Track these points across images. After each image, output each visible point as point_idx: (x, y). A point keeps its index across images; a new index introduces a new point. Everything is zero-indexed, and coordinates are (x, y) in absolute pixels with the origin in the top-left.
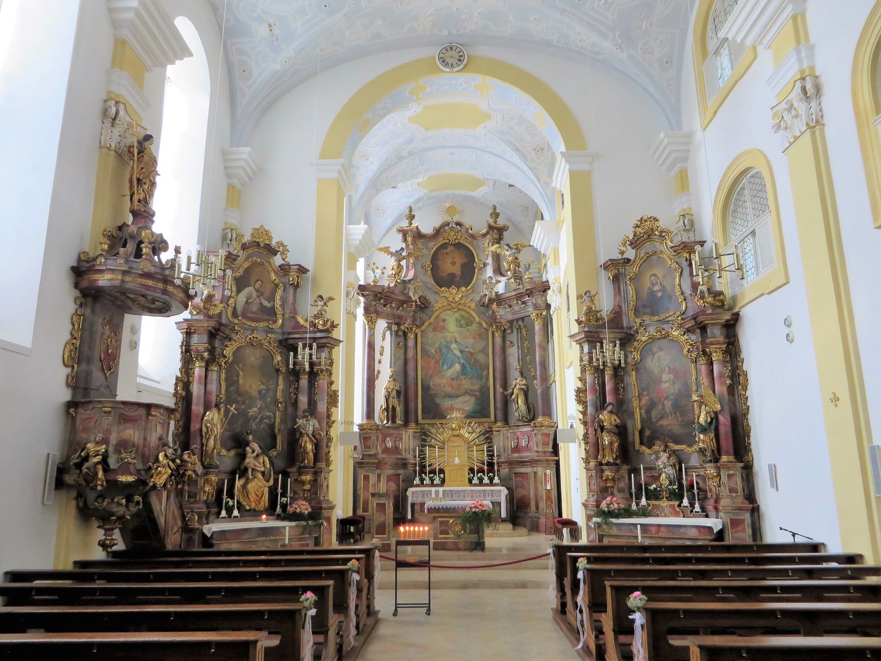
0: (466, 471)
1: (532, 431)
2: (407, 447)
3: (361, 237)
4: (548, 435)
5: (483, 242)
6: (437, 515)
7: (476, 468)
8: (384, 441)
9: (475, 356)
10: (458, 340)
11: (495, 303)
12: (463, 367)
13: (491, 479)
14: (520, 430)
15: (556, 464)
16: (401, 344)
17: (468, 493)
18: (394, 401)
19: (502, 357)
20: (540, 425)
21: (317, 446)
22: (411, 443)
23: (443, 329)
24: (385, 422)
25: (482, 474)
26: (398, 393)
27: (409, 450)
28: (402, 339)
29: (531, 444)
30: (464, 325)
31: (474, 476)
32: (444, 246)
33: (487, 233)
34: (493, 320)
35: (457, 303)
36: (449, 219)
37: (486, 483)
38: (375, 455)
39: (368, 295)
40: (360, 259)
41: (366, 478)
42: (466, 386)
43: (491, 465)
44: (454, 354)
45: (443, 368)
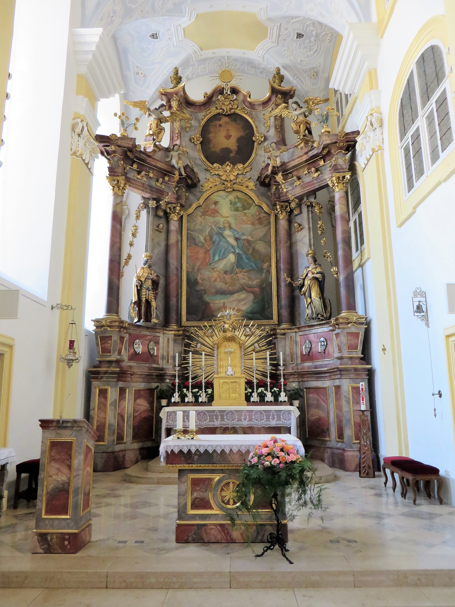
0: (243, 385)
2: (165, 354)
3: (94, 48)
4: (356, 335)
5: (263, 112)
6: (186, 467)
7: (255, 381)
8: (132, 343)
10: (233, 226)
11: (280, 174)
12: (239, 257)
13: (276, 396)
14: (314, 331)
16: (161, 225)
17: (245, 415)
18: (147, 294)
19: (288, 244)
20: (345, 321)
21: (318, 439)
23: (215, 212)
24: (136, 320)
25: (263, 389)
26: (155, 284)
27: (168, 356)
28: (163, 221)
29: (329, 348)
30: (240, 209)
31: (253, 392)
32: (216, 117)
33: (269, 99)
34: (277, 198)
36: (224, 85)
37: (269, 401)
38: (118, 362)
39: (114, 152)
40: (100, 99)
41: (103, 393)
42: (242, 281)
43: (275, 377)
44: (227, 242)
45: (213, 259)
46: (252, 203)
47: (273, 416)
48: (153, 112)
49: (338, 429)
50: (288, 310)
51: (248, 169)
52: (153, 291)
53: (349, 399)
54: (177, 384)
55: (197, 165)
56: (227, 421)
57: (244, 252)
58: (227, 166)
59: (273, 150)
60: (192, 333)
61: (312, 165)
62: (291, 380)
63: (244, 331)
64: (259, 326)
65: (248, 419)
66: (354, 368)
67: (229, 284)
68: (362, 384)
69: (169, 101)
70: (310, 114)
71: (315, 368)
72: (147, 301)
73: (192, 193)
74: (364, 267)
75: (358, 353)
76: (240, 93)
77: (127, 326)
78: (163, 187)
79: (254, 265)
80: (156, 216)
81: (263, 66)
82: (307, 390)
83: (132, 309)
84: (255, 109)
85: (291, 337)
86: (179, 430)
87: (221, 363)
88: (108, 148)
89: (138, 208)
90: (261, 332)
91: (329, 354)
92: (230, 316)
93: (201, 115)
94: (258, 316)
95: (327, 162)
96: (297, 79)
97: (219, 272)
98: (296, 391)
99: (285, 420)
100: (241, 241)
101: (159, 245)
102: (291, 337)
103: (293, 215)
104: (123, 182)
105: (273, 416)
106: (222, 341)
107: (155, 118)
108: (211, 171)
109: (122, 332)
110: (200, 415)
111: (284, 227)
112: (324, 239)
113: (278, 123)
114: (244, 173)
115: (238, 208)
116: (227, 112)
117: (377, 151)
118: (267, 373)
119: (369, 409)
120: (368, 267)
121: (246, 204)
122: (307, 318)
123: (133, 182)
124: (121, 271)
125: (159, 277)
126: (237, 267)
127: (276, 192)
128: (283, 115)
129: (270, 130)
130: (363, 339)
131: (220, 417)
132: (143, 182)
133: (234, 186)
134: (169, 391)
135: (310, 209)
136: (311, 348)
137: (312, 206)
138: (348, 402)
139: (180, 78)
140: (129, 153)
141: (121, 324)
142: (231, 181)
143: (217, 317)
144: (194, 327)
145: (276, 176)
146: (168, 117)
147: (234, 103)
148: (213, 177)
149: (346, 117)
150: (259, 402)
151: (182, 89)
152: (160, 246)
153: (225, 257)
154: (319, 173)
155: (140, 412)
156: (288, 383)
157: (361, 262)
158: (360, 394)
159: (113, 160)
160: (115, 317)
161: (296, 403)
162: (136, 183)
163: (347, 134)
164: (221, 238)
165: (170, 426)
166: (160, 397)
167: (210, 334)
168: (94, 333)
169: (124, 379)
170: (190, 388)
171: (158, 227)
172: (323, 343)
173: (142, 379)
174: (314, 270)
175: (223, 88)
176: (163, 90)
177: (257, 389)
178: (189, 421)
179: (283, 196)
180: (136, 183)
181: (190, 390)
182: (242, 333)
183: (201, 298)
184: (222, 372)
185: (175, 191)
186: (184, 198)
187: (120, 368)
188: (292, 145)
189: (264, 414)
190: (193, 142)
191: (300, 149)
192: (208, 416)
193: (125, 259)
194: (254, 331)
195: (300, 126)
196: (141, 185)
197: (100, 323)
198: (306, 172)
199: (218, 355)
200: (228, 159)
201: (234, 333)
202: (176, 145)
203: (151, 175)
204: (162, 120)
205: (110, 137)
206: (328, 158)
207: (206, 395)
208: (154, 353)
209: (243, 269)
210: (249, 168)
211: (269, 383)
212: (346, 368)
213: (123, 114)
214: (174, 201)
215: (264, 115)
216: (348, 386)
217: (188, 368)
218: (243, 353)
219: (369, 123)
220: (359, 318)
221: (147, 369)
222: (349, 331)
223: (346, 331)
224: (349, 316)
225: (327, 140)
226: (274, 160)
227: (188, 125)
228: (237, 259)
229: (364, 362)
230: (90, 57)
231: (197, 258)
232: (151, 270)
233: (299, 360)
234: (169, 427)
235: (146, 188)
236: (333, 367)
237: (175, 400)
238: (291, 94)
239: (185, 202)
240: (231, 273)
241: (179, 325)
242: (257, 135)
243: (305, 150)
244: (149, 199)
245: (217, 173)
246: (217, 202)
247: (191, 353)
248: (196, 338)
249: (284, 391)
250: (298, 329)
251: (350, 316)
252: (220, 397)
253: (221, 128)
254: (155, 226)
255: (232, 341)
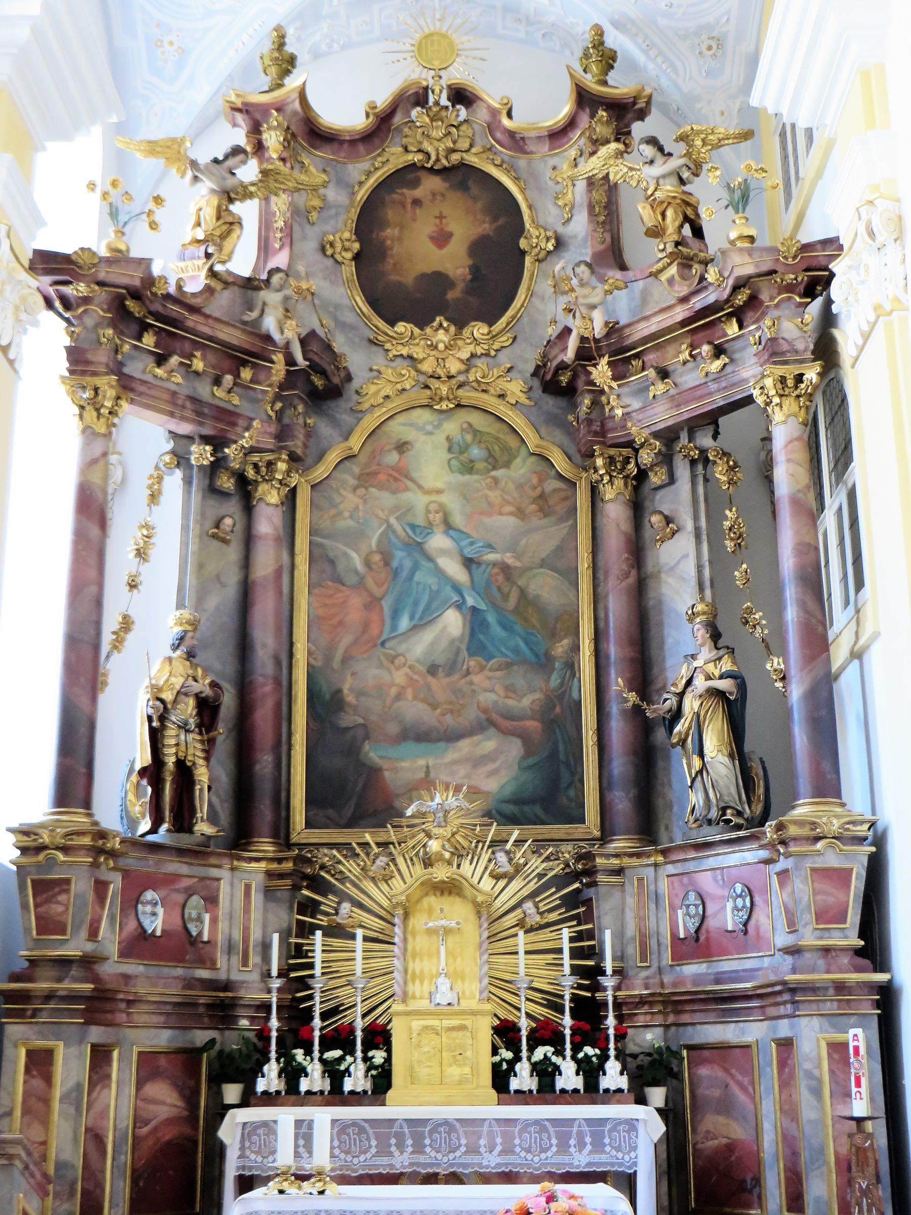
0: (486, 1037)
1: (767, 862)
4: (842, 877)
5: (552, 162)
7: (525, 1025)
8: (131, 901)
9: (521, 582)
10: (458, 520)
11: (604, 361)
14: (711, 862)
15: (878, 1004)
16: (228, 521)
17: (491, 1136)
19: (632, 580)
20: (805, 831)
22: (256, 915)
24: (145, 825)
25: (549, 1050)
28: (233, 507)
29: (761, 918)
30: (481, 466)
33: (571, 124)
34: (596, 434)
35: (454, 381)
36: (426, 78)
37: (569, 1087)
38: (88, 962)
39: (86, 300)
40: (48, 144)
42: (487, 698)
44: (440, 573)
45: (394, 627)
46: (519, 447)
47: (580, 1136)
48: (207, 171)
49: (787, 1179)
50: (633, 792)
51: (504, 338)
52: (201, 733)
53: (820, 1080)
54: (274, 1034)
55: (342, 326)
56: (433, 1154)
57: (494, 605)
58: (437, 330)
59: (582, 284)
60: (323, 867)
61: (701, 335)
62: (641, 1020)
63: (490, 860)
64: (540, 844)
65: (499, 1148)
66: (834, 982)
67: (445, 706)
68: (855, 1035)
69: (255, 130)
70: (697, 175)
71: (718, 981)
72: (180, 764)
73: (326, 415)
74: (866, 658)
75: (848, 933)
76: (479, 103)
77: (117, 846)
78: (236, 401)
79: (522, 645)
80: (213, 490)
81: (552, 19)
82: (693, 1053)
83: (132, 789)
84: (525, 152)
85: (640, 880)
86: (284, 1169)
87: (415, 966)
88: (68, 290)
89: (157, 468)
90: (545, 865)
91: (758, 936)
92: (446, 812)
93: (356, 170)
94: (538, 810)
95: (748, 326)
96: (659, 60)
97: (410, 667)
98: (656, 1056)
99: (618, 1149)
100: (483, 567)
101: (221, 583)
102: (640, 880)
103: (646, 489)
104: (111, 393)
105: (580, 1136)
106: (419, 893)
107: (213, 191)
108: (388, 346)
109: (103, 867)
110: (348, 1135)
111: (618, 525)
112: (744, 566)
113: (599, 195)
114: (493, 353)
115: (472, 461)
116: (438, 160)
117: (890, 313)
118: (562, 997)
119: (881, 1112)
120: (875, 658)
121: (496, 448)
122: (692, 819)
123: (142, 389)
124: (102, 671)
125: (220, 688)
126: (472, 653)
127: (593, 416)
128: (611, 177)
129: (574, 218)
130: (863, 888)
131: (409, 1142)
132: (173, 387)
133: (460, 392)
134: (248, 1056)
135: (700, 468)
136: (703, 918)
137: (706, 461)
138: (817, 1092)
139: (292, 61)
140: (129, 303)
141: (101, 842)
142: (450, 377)
143: (401, 815)
144: (331, 846)
145: (590, 369)
146: (253, 184)
147: (461, 133)
148: (394, 364)
149: (807, 184)
150: (538, 1091)
151: (295, 95)
152: (224, 585)
153: (430, 621)
154: (724, 359)
155: (153, 1124)
156: (630, 1031)
157: (856, 643)
158: (847, 1064)
159: (82, 323)
160: (79, 819)
161: (657, 1095)
162: (153, 392)
163: (806, 247)
164: (418, 556)
165: (251, 1168)
166: (218, 1079)
167: (383, 872)
168: (14, 868)
169: (109, 1016)
170: (316, 1047)
171: (217, 527)
172: (740, 902)
173: (162, 1019)
174: (710, 668)
175: (426, 89)
176: (238, 96)
177: (531, 1050)
178: (310, 1153)
179: (614, 429)
180: (153, 392)
181: (316, 1054)
182: (486, 868)
183: (352, 751)
184: (418, 995)
185: (271, 413)
186: (300, 434)
187: (92, 982)
188: (642, 271)
189: (551, 1130)
190: (332, 256)
191: (666, 284)
192: (372, 1136)
193: (114, 633)
194: (522, 861)
195: (663, 215)
196: (167, 397)
197: (34, 837)
198: (685, 355)
199: (405, 940)
200: (441, 308)
201: (459, 866)
202: (278, 270)
203: (198, 365)
204: (233, 195)
205: (74, 258)
206: (750, 316)
207: (368, 1070)
208: (200, 934)
209: (488, 660)
210: (509, 335)
211: (568, 1032)
212: (812, 982)
213: (114, 184)
214: (269, 442)
215: (554, 168)
216: (818, 1040)
217: (310, 982)
218: (486, 934)
219: (862, 230)
220: (848, 823)
221: (180, 986)
222: (819, 863)
223: (809, 864)
224: (815, 817)
225: (745, 267)
226: (584, 318)
227: (316, 203)
228: (468, 625)
229: (866, 962)
230: (24, 33)
231: (341, 623)
232: (194, 666)
233: (667, 958)
234: (247, 1173)
235: (183, 407)
236: (773, 978)
237: (269, 1084)
238: (637, 106)
239: (305, 446)
240: (449, 674)
241: (281, 841)
242: (534, 232)
243: (683, 289)
244: (190, 438)
245: (405, 351)
246: (406, 443)
247: (319, 933)
248: (334, 885)
249: (617, 1058)
250: (665, 857)
251: (820, 817)
252: (413, 1078)
253: (418, 211)
254: (208, 524)
255: (450, 893)
